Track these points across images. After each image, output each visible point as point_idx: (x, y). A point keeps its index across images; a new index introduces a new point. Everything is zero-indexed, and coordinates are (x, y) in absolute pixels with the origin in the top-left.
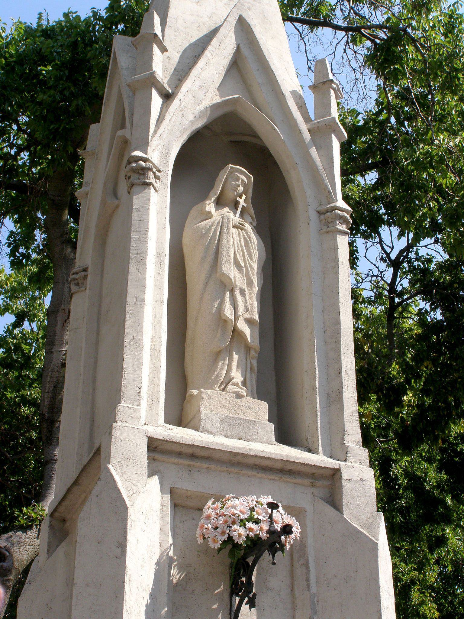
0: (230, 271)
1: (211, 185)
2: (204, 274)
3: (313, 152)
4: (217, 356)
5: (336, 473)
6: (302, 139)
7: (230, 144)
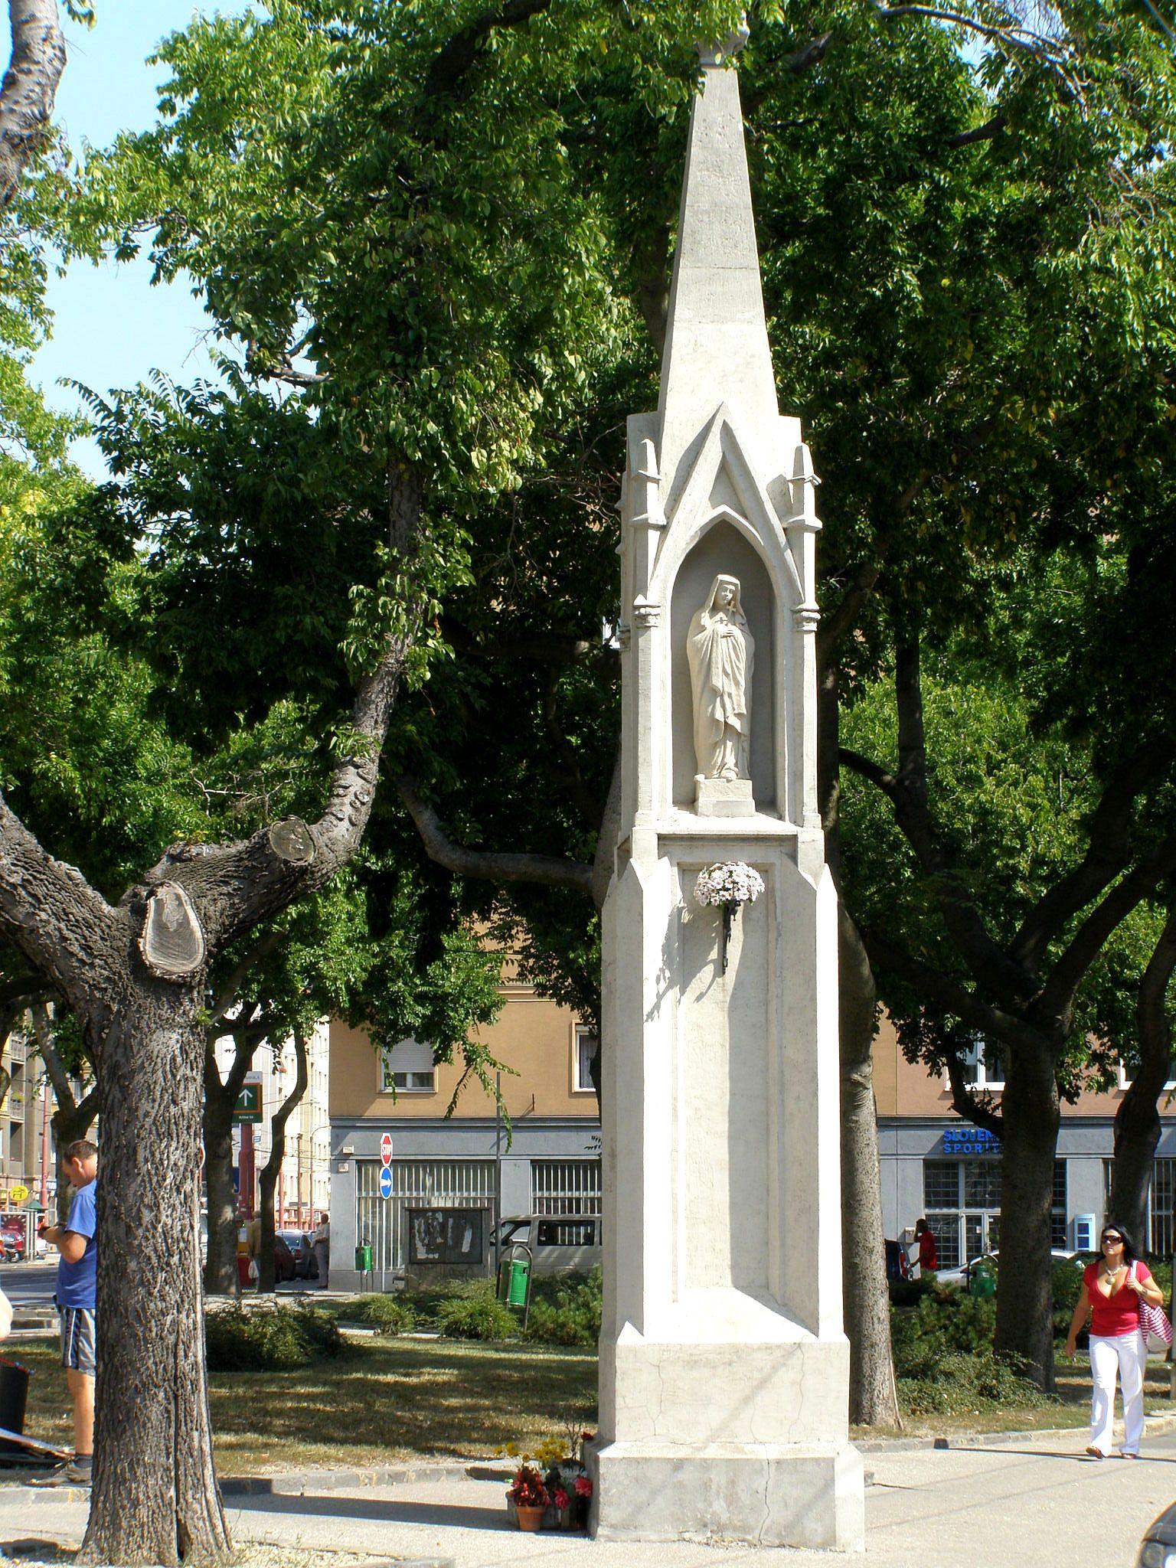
0: (719, 681)
1: (707, 596)
2: (700, 683)
3: (788, 554)
4: (715, 745)
5: (794, 838)
6: (778, 543)
7: (721, 547)
